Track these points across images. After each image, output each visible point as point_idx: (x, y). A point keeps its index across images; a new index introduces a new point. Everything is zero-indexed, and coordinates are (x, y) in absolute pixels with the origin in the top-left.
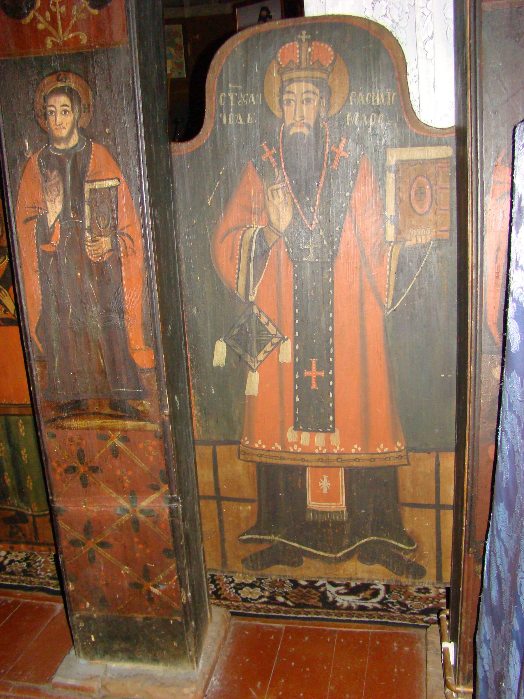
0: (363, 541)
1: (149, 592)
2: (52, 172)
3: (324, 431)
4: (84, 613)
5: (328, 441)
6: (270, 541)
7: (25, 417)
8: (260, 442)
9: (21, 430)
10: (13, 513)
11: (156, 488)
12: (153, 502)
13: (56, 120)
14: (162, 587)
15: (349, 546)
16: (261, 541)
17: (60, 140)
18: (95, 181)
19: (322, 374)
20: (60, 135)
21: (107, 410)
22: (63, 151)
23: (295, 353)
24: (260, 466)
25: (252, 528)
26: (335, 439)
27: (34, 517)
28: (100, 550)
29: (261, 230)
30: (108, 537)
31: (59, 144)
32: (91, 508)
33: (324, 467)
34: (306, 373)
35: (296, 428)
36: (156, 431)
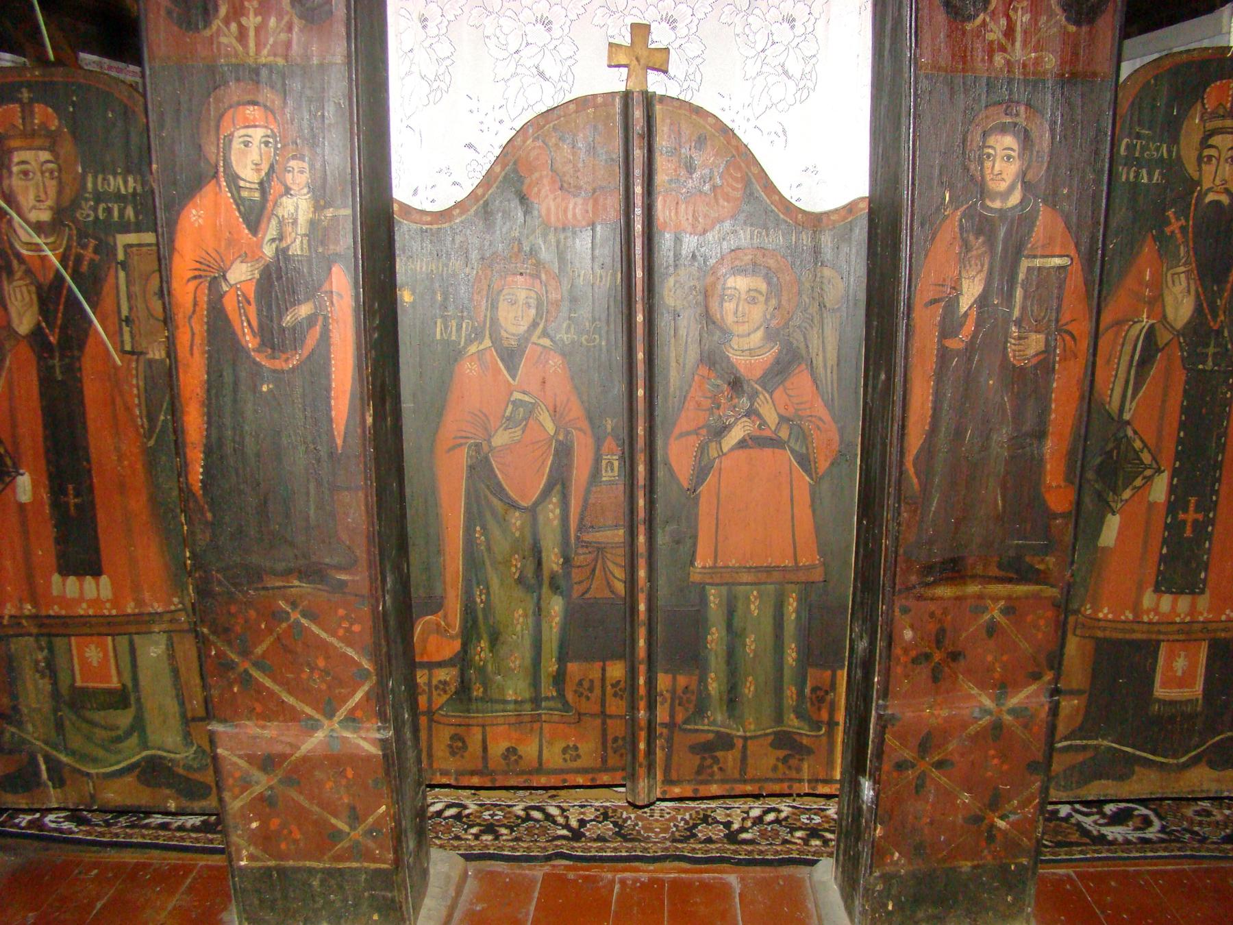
0: (1218, 738)
1: (992, 826)
3: (1192, 593)
5: (1193, 605)
6: (1096, 747)
7: (763, 587)
8: (1106, 610)
9: (752, 607)
10: (711, 736)
11: (1036, 677)
12: (1028, 697)
14: (1012, 818)
15: (1197, 747)
16: (1084, 748)
18: (1035, 257)
19: (1200, 517)
20: (998, 189)
21: (994, 571)
22: (995, 211)
23: (1172, 489)
24: (1099, 642)
25: (1073, 732)
26: (1203, 602)
27: (745, 739)
28: (935, 773)
29: (1152, 326)
30: (951, 753)
31: (993, 200)
33: (1184, 641)
34: (1181, 516)
35: (1157, 590)
36: (1055, 598)
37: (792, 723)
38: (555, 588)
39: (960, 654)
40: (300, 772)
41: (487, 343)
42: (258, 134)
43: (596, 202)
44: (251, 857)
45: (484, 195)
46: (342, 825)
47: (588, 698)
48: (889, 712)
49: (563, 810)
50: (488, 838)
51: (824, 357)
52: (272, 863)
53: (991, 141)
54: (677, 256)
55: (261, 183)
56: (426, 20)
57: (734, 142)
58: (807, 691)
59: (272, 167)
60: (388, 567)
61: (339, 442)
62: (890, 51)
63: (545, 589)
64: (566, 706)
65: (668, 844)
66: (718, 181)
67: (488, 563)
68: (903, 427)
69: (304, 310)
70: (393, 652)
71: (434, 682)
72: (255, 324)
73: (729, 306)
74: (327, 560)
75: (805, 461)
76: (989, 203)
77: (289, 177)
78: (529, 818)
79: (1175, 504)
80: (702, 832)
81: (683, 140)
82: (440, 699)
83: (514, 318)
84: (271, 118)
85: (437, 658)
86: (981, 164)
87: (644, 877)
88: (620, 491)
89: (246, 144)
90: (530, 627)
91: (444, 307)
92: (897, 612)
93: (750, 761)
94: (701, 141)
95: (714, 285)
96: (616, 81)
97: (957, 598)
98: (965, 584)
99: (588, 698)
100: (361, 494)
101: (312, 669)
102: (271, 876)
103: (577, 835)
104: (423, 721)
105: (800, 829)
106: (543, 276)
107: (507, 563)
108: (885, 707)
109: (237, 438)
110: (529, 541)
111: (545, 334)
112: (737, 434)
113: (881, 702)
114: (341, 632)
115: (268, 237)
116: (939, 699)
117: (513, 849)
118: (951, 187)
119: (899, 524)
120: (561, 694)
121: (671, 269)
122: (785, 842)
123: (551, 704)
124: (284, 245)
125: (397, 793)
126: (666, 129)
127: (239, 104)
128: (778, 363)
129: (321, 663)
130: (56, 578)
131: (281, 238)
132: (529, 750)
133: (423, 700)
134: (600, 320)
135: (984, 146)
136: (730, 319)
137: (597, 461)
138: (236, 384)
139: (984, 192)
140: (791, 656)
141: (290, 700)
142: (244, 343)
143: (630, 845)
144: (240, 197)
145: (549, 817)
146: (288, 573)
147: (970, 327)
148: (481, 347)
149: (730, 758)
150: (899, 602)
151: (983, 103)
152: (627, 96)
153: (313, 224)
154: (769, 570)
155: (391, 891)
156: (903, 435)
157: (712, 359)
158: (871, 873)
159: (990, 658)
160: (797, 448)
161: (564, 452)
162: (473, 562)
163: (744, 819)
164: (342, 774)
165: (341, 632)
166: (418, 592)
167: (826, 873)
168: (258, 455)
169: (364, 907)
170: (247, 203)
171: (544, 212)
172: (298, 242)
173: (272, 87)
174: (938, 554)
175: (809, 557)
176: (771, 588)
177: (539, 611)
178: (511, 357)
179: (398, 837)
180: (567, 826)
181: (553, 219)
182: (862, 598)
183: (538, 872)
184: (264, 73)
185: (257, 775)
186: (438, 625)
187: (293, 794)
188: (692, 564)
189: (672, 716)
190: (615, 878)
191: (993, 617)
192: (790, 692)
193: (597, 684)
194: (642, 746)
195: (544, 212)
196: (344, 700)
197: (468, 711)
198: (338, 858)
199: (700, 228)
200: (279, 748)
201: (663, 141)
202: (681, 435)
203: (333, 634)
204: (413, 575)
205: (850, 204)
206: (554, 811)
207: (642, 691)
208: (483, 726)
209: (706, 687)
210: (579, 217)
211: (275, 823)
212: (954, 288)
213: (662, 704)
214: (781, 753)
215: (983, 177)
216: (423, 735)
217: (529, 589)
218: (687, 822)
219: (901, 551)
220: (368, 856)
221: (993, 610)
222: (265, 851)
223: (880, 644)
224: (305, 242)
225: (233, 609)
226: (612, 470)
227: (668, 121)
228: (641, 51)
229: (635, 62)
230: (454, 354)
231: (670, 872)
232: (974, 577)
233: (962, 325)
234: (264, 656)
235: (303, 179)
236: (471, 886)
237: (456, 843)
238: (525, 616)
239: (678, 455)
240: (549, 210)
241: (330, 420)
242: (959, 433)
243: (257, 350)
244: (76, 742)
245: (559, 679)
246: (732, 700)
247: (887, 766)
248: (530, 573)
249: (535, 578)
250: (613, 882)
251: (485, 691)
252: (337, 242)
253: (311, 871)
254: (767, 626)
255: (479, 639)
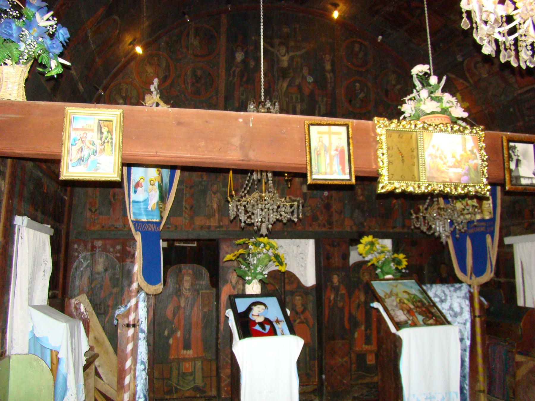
79: (366, 330)
112: (298, 321)
130: (182, 351)
140: (308, 359)
147: (332, 302)
244: (181, 383)
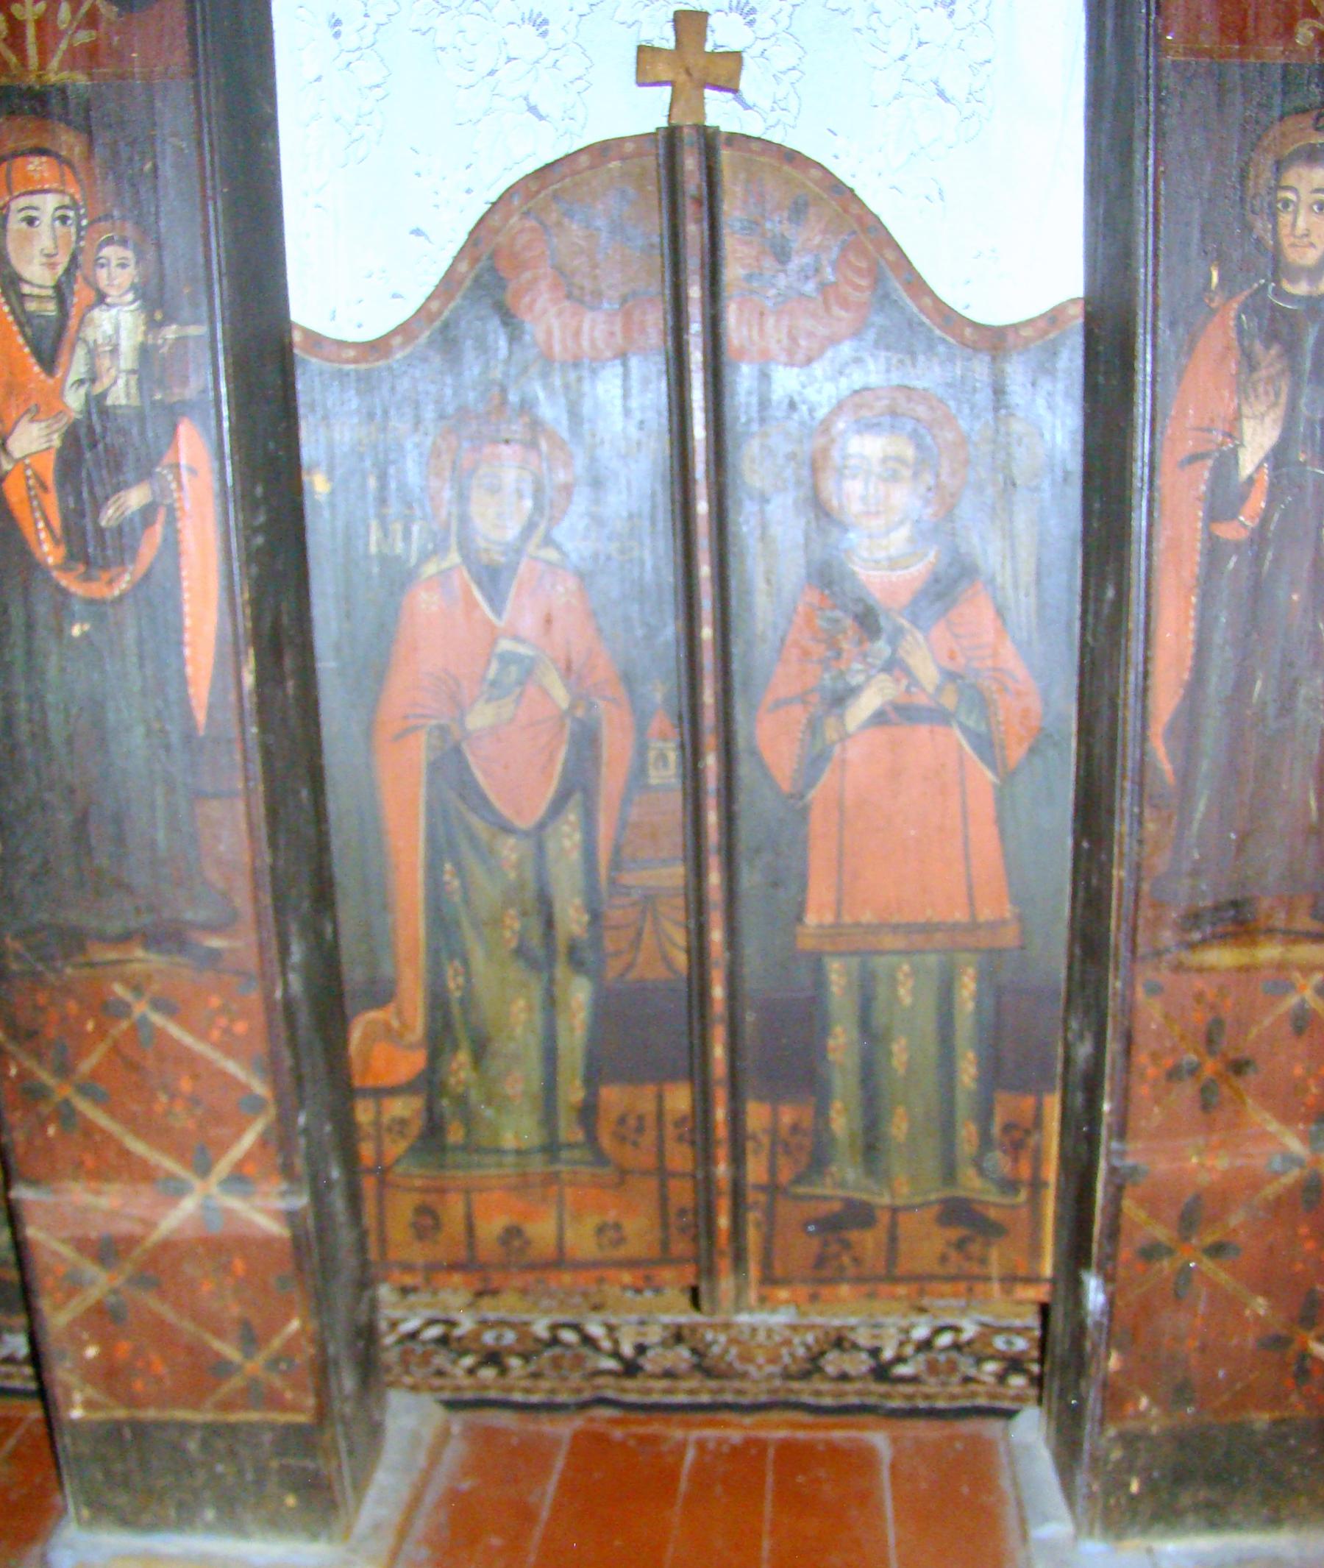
2: (1267, 348)
4: (1132, 1425)
9: (902, 991)
13: (1294, 225)
17: (1296, 273)
21: (1304, 922)
27: (894, 1210)
31: (1293, 281)
32: (1209, 1163)
37: (972, 1184)
38: (577, 962)
39: (1247, 1063)
40: (160, 1265)
41: (454, 558)
42: (49, 204)
43: (628, 316)
44: (89, 1405)
45: (440, 313)
46: (230, 1351)
47: (635, 1144)
48: (1129, 1161)
49: (611, 1329)
50: (488, 1373)
51: (1015, 570)
52: (121, 1413)
53: (1291, 178)
54: (764, 404)
55: (58, 288)
56: (338, 23)
57: (854, 209)
58: (996, 1129)
59: (74, 259)
60: (294, 927)
61: (201, 717)
62: (1115, 32)
63: (561, 969)
64: (600, 1158)
65: (777, 1383)
66: (829, 275)
67: (465, 923)
68: (1146, 675)
69: (135, 498)
70: (307, 1070)
71: (386, 1119)
72: (57, 523)
73: (854, 487)
74: (189, 915)
75: (986, 746)
76: (1287, 287)
77: (102, 274)
78: (555, 1341)
80: (833, 1362)
81: (768, 207)
82: (396, 1148)
83: (498, 518)
84: (69, 177)
85: (387, 1081)
86: (1274, 216)
87: (736, 1436)
88: (674, 803)
89: (31, 221)
90: (538, 1026)
91: (382, 501)
92: (1140, 993)
93: (903, 1247)
94: (798, 210)
95: (825, 451)
96: (648, 111)
97: (1246, 969)
98: (1254, 943)
99: (635, 1144)
100: (241, 806)
101: (173, 1097)
102: (121, 1435)
103: (631, 1369)
104: (369, 1185)
105: (992, 1358)
106: (544, 446)
107: (497, 922)
108: (1122, 1154)
109: (37, 716)
110: (532, 887)
111: (548, 541)
113: (1115, 1145)
114: (216, 1034)
115: (73, 377)
116: (1215, 1138)
117: (527, 1391)
118: (1222, 260)
119: (1140, 842)
120: (592, 1138)
121: (755, 427)
122: (967, 1380)
123: (577, 1154)
124: (98, 389)
125: (320, 1303)
126: (738, 190)
127: (15, 155)
128: (937, 581)
129: (186, 1085)
131: (93, 378)
132: (542, 1230)
133: (367, 1150)
134: (640, 515)
135: (1279, 187)
136: (855, 507)
137: (642, 750)
138: (30, 626)
139: (1278, 266)
140: (968, 1071)
141: (137, 1147)
142: (38, 555)
143: (713, 1384)
144: (24, 311)
145: (588, 1340)
146: (125, 938)
147: (1258, 502)
148: (445, 565)
149: (869, 1241)
150: (1146, 973)
151: (1276, 113)
152: (671, 137)
153: (145, 352)
154: (928, 929)
155: (313, 1457)
156: (1145, 690)
157: (827, 577)
158: (1101, 1432)
159: (1298, 1070)
160: (971, 723)
161: (586, 742)
162: (442, 923)
163: (902, 1344)
164: (226, 1268)
165: (216, 1034)
166: (354, 974)
167: (1030, 1431)
168: (69, 741)
169: (272, 1485)
170: (36, 322)
171: (541, 337)
172: (121, 382)
173: (69, 123)
174: (1207, 893)
175: (994, 907)
176: (932, 960)
177: (551, 1003)
178: (492, 579)
179: (323, 1369)
180: (616, 1354)
181: (557, 348)
182: (1083, 972)
183: (563, 1429)
184: (55, 102)
185: (91, 1270)
186: (388, 1027)
187: (152, 1302)
188: (799, 919)
189: (773, 1169)
190: (690, 1438)
191: (1303, 1001)
192: (967, 1133)
193: (650, 1122)
194: (723, 1222)
195: (541, 337)
196: (224, 1147)
197: (442, 1166)
198: (226, 1406)
199: (800, 356)
200: (124, 1227)
201: (733, 211)
202: (779, 704)
203: (203, 1035)
204: (343, 942)
205: (1054, 310)
206: (596, 1330)
207: (722, 1131)
208: (467, 1192)
209: (827, 1121)
210: (600, 344)
211: (124, 1348)
212: (1230, 436)
213: (756, 1153)
214: (954, 1233)
215: (1277, 244)
216: (370, 1208)
217: (533, 964)
218: (808, 1348)
219: (1145, 887)
220: (273, 1401)
221: (1303, 987)
222: (111, 1392)
223: (1113, 1046)
224: (133, 383)
225: (42, 998)
226: (665, 764)
227: (742, 176)
228: (689, 58)
229: (682, 77)
230: (399, 578)
231: (776, 1430)
232: (1270, 932)
233: (1243, 498)
234: (94, 1075)
235: (126, 277)
236: (456, 1451)
237: (437, 1382)
238: (529, 1008)
239: (772, 737)
240: (549, 333)
241: (184, 681)
242: (1242, 685)
243: (65, 567)
245: (588, 1113)
246: (871, 1146)
247: (1125, 1253)
248: (535, 940)
249: (544, 951)
250: (682, 1446)
251: (468, 1134)
252: (185, 381)
253: (185, 1427)
254: (927, 1022)
255: (456, 1047)
